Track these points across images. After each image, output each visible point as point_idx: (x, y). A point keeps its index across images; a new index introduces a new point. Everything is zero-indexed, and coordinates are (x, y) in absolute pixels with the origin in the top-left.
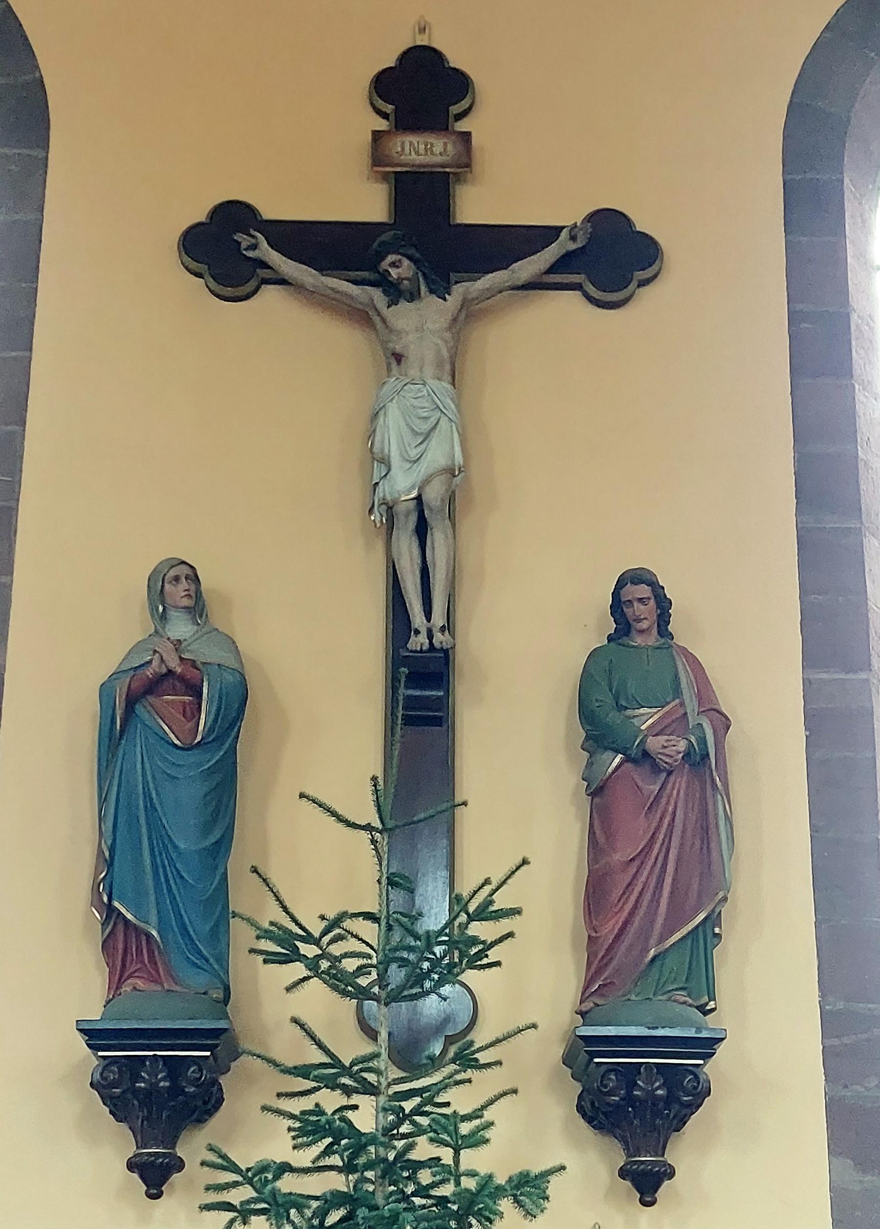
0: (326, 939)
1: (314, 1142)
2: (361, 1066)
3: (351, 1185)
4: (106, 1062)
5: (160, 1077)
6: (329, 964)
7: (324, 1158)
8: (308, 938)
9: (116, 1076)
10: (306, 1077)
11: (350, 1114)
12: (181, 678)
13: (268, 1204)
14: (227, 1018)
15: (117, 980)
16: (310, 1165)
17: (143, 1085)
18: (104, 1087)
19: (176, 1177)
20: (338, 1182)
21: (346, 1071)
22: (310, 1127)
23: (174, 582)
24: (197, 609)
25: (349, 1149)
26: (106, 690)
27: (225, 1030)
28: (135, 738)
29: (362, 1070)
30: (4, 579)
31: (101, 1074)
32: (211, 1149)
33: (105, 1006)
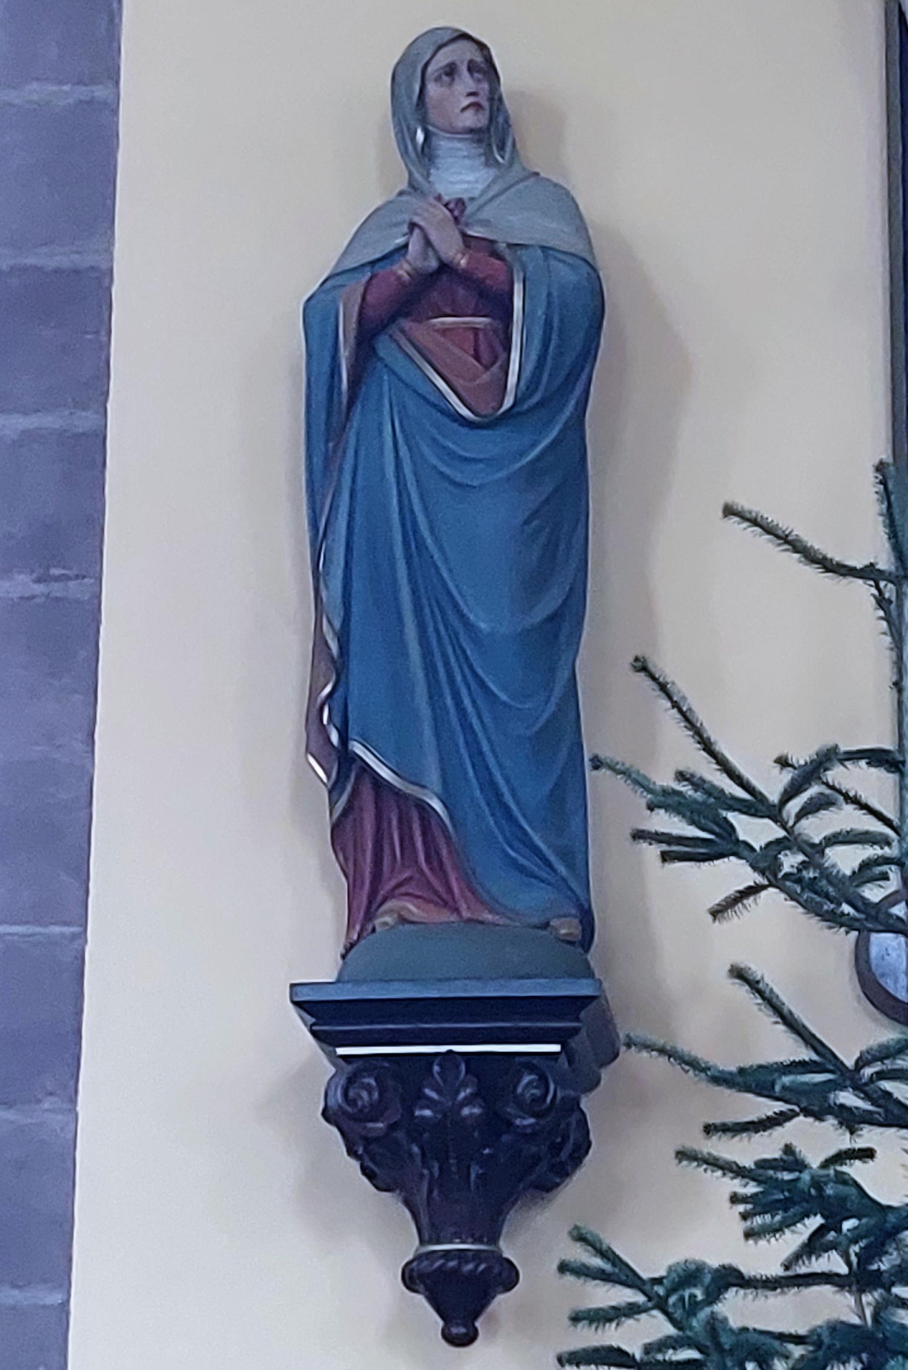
0: (794, 806)
1: (787, 1223)
2: (877, 1067)
3: (868, 1313)
4: (349, 1068)
5: (462, 1095)
6: (801, 858)
7: (809, 1258)
8: (756, 805)
9: (376, 1095)
10: (764, 1090)
11: (855, 1170)
12: (465, 277)
13: (701, 1352)
14: (590, 974)
15: (365, 902)
16: (780, 1272)
17: (427, 1113)
18: (351, 1117)
19: (501, 1302)
20: (839, 1307)
21: (849, 1078)
22: (777, 1194)
23: (445, 78)
24: (493, 132)
25: (862, 1238)
26: (317, 313)
27: (592, 998)
28: (379, 410)
29: (881, 1075)
30: (100, 92)
31: (345, 1094)
32: (580, 1237)
33: (343, 957)
